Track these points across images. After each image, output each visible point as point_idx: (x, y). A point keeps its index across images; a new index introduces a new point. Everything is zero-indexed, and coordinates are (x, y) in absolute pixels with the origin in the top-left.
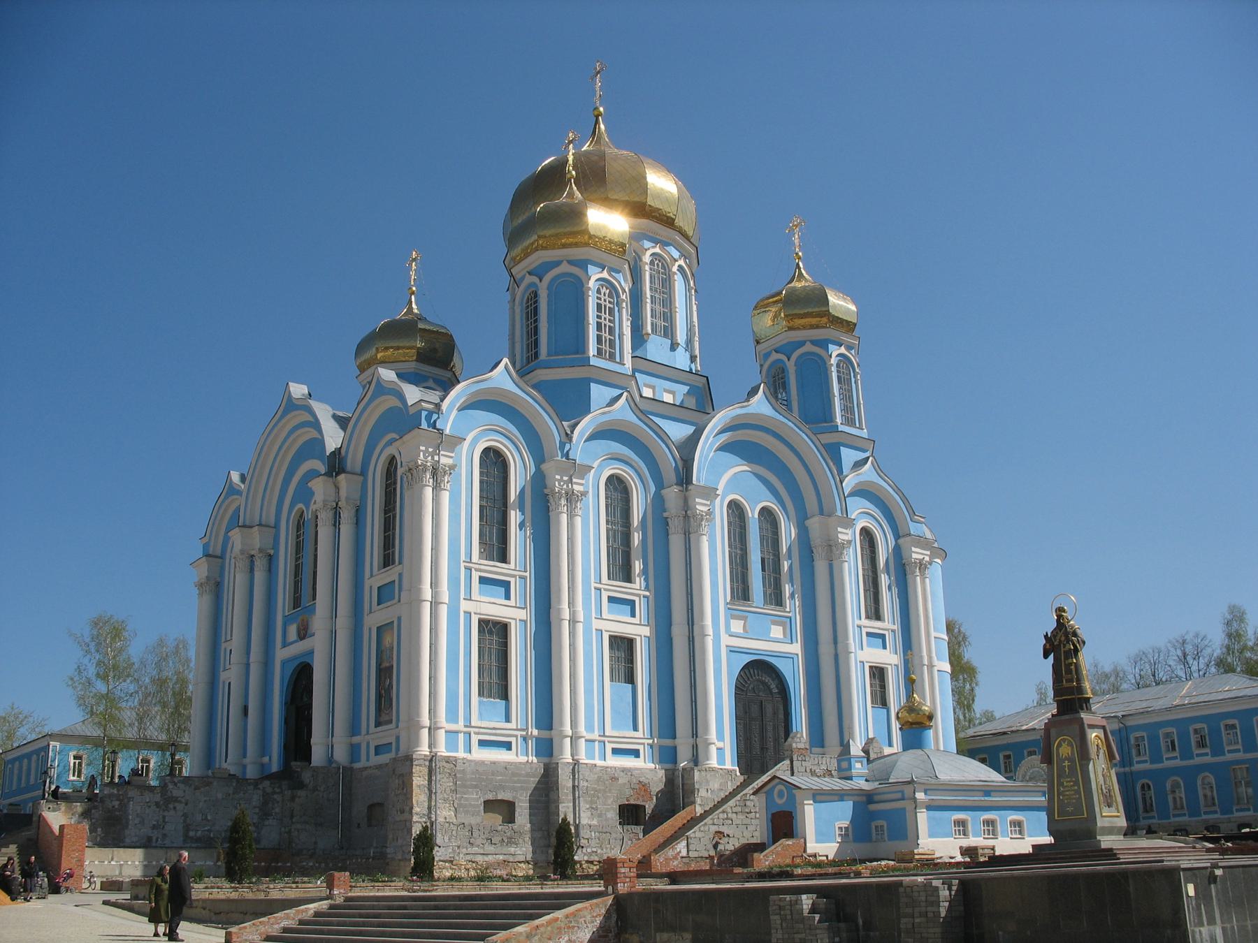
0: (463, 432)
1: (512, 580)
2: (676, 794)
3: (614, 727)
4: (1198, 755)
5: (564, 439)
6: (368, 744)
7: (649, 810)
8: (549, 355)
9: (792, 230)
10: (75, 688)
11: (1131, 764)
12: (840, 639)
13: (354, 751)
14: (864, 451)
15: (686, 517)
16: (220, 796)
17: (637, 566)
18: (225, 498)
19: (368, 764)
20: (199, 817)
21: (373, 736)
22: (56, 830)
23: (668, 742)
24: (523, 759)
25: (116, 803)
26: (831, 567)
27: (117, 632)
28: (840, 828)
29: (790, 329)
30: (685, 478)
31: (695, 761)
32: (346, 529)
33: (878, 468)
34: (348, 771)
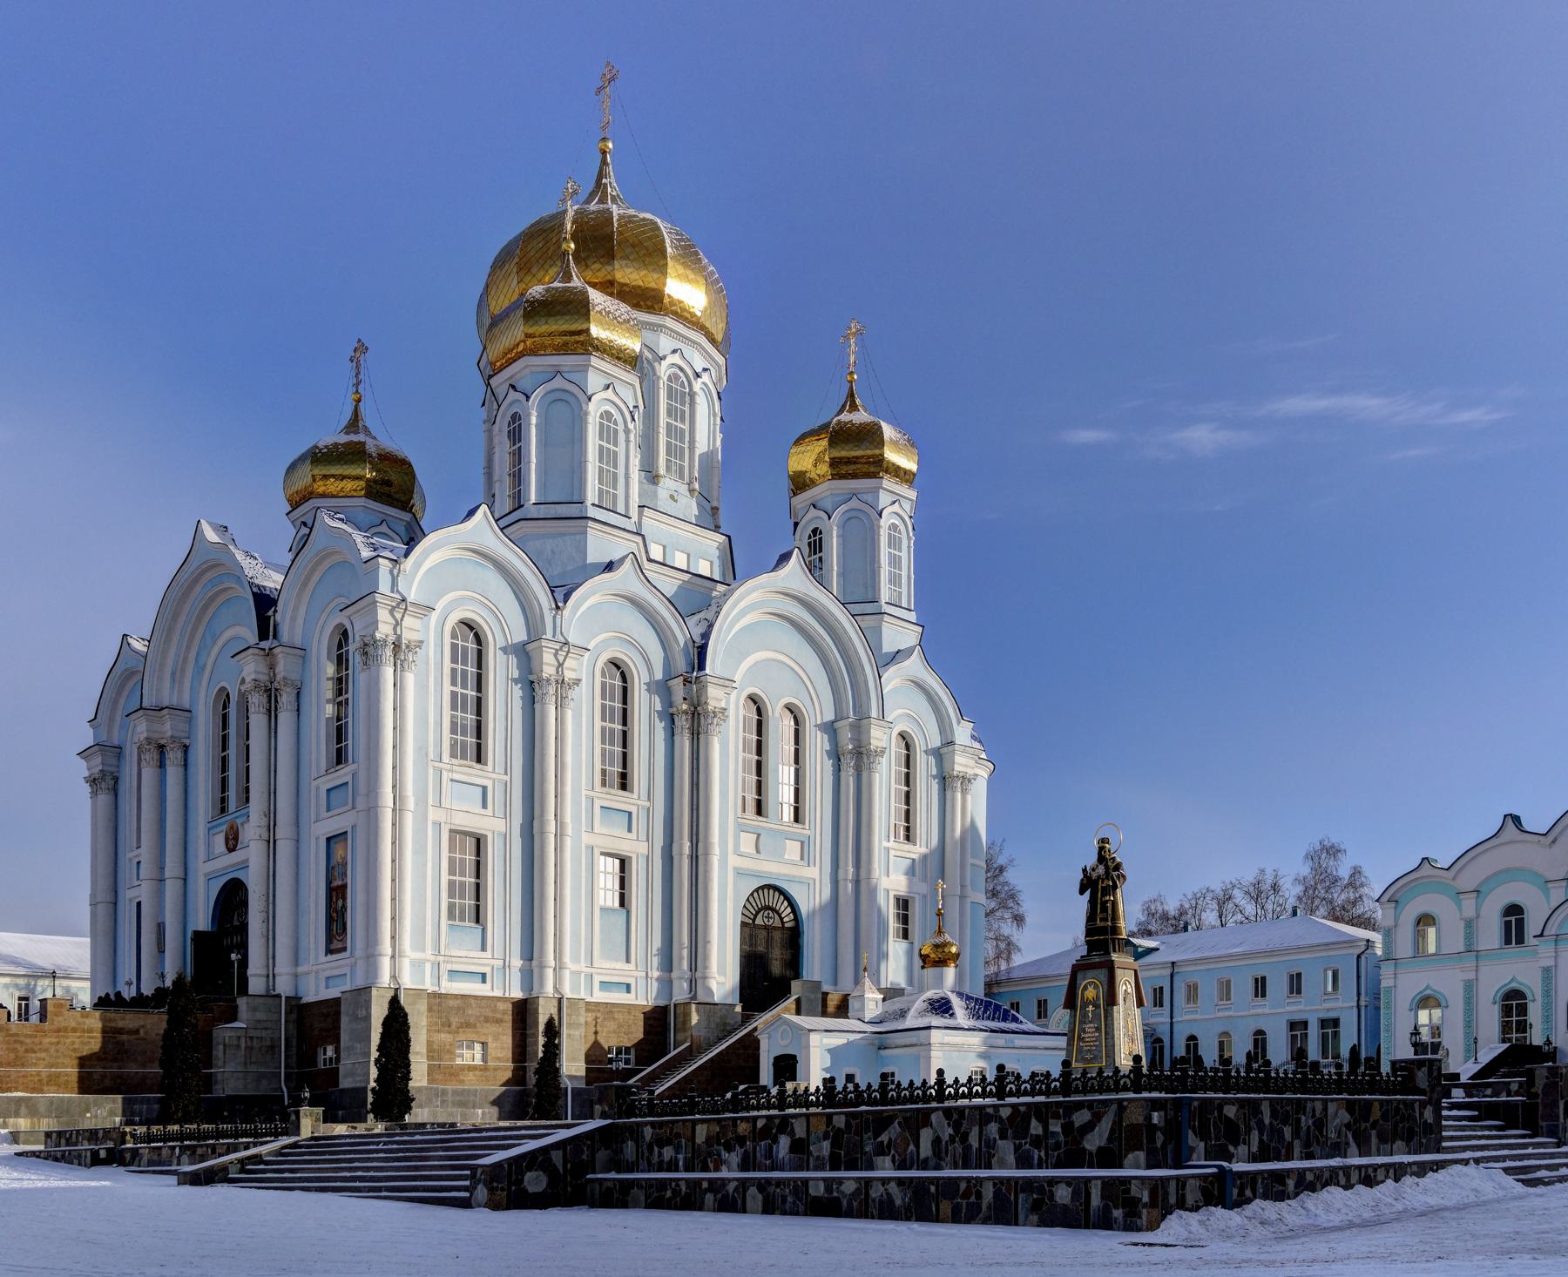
9: (847, 338)
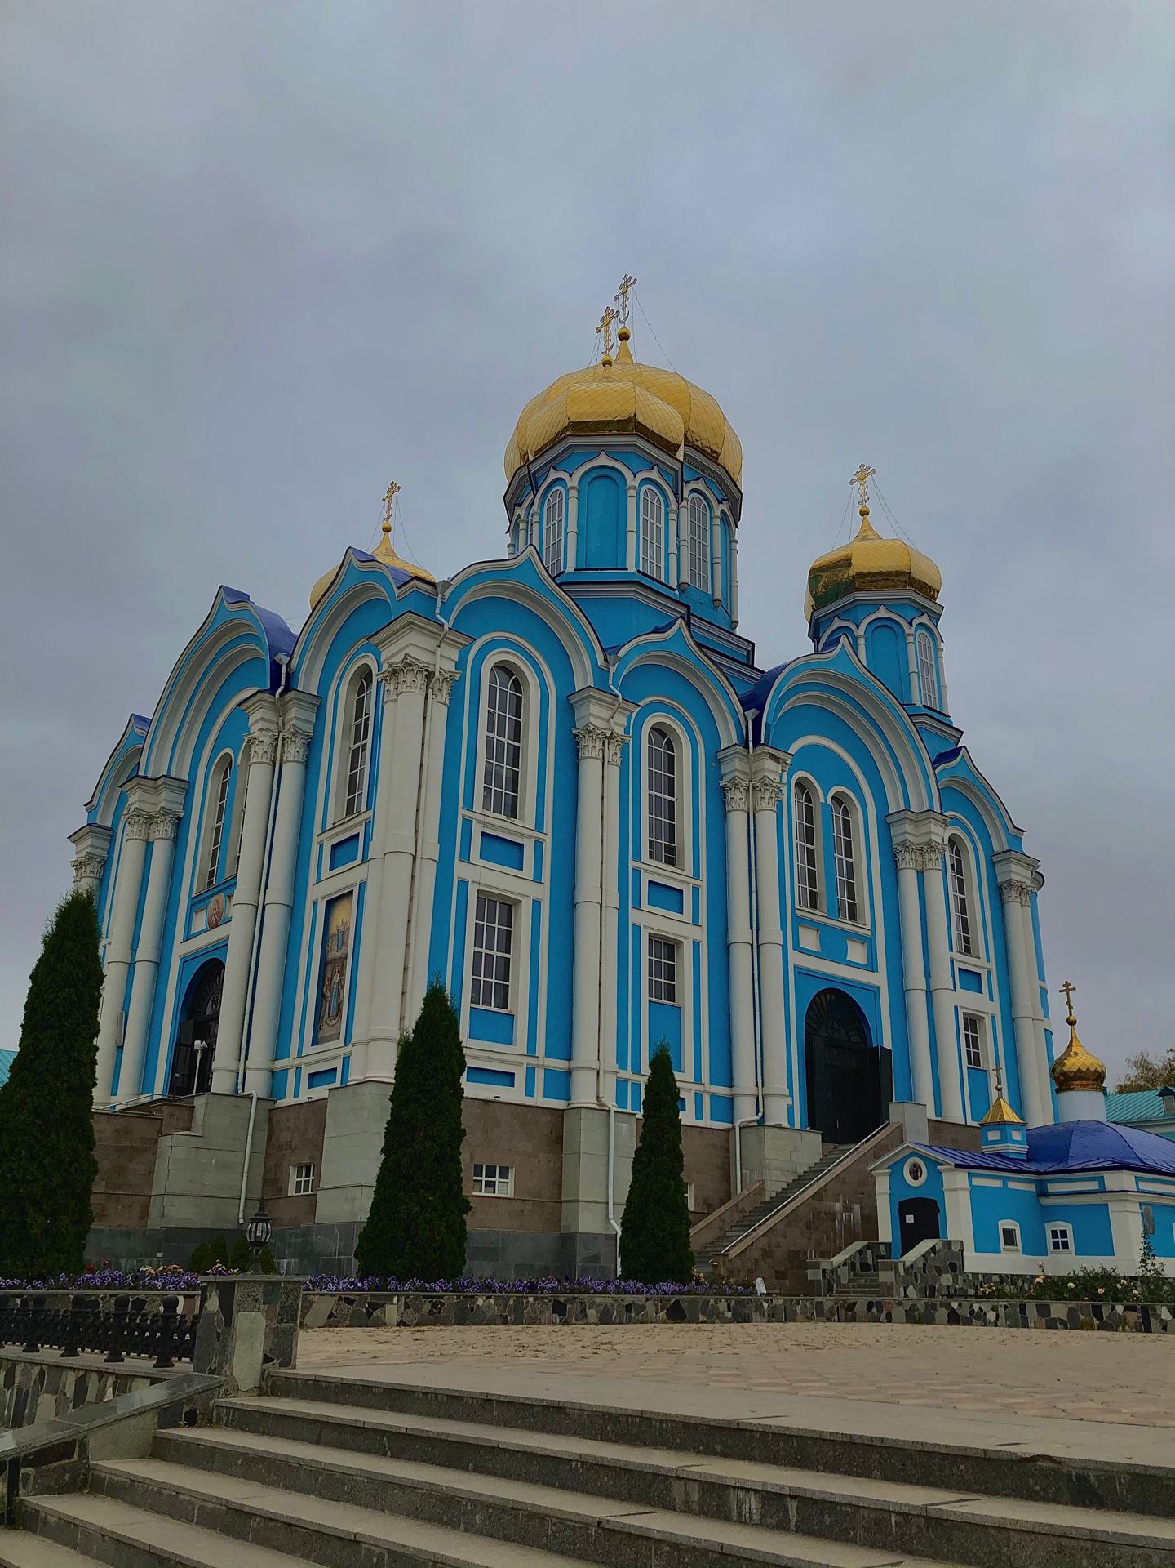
6: (299, 1069)
13: (276, 1078)
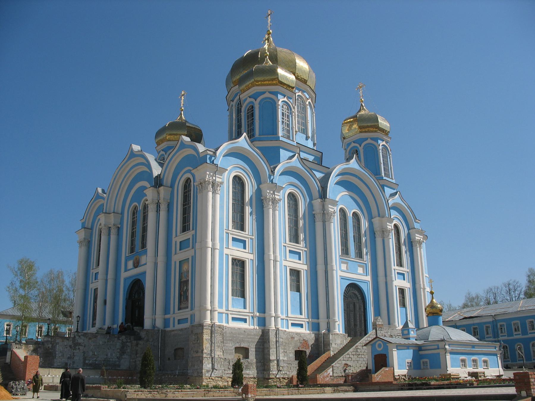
0: (226, 166)
1: (247, 240)
2: (320, 345)
3: (292, 313)
4: (530, 333)
5: (271, 173)
6: (174, 319)
7: (308, 353)
8: (260, 135)
10: (10, 292)
11: (498, 337)
12: (388, 274)
13: (166, 322)
14: (394, 189)
15: (324, 214)
16: (101, 343)
17: (302, 236)
18: (95, 201)
19: (174, 329)
20: (91, 354)
21: (177, 315)
22: (23, 359)
23: (315, 321)
24: (252, 327)
25: (50, 346)
26: (383, 241)
27: (30, 267)
28: (408, 363)
29: (361, 132)
30: (323, 195)
31: (328, 330)
32: (163, 214)
33: (401, 197)
34: (164, 332)
